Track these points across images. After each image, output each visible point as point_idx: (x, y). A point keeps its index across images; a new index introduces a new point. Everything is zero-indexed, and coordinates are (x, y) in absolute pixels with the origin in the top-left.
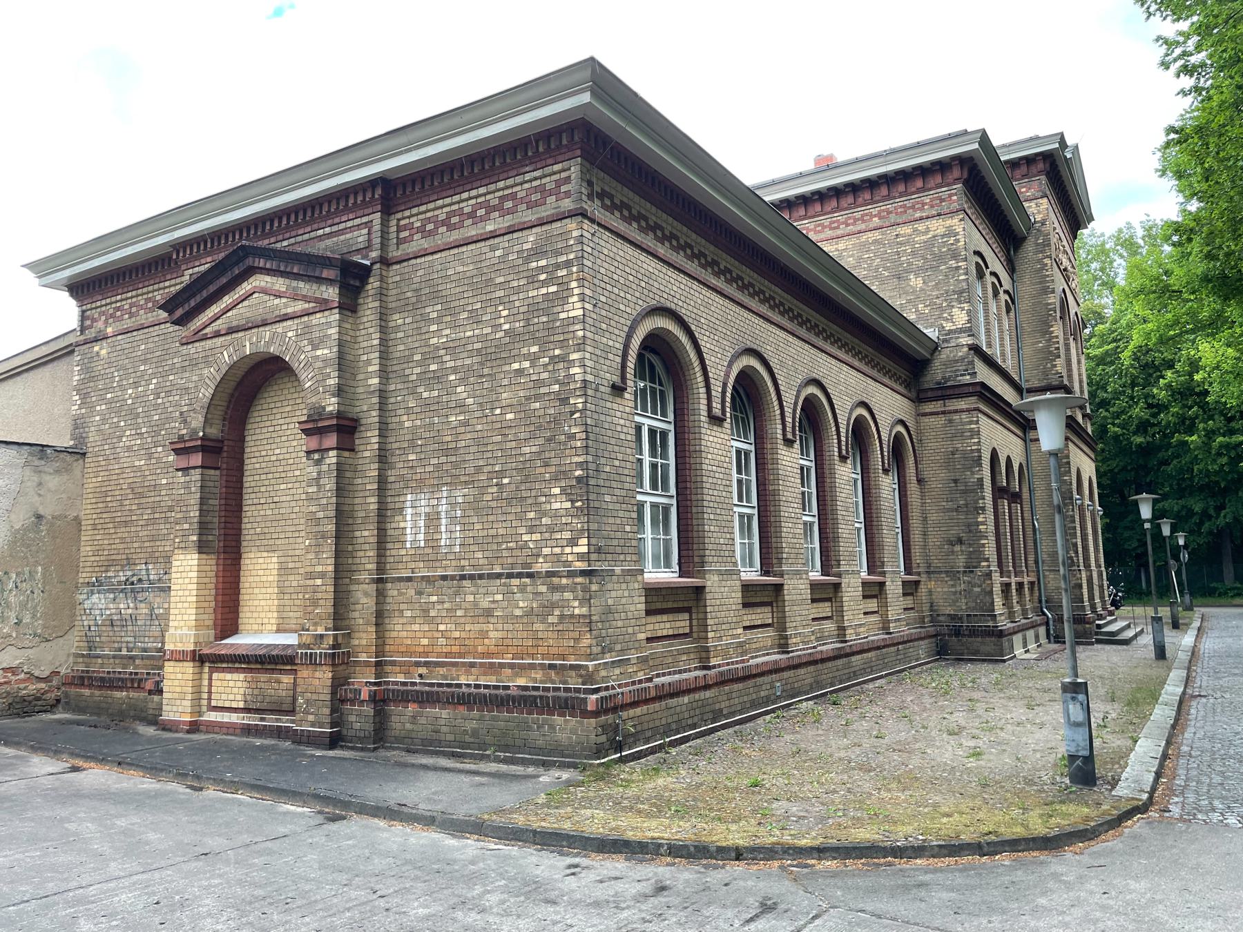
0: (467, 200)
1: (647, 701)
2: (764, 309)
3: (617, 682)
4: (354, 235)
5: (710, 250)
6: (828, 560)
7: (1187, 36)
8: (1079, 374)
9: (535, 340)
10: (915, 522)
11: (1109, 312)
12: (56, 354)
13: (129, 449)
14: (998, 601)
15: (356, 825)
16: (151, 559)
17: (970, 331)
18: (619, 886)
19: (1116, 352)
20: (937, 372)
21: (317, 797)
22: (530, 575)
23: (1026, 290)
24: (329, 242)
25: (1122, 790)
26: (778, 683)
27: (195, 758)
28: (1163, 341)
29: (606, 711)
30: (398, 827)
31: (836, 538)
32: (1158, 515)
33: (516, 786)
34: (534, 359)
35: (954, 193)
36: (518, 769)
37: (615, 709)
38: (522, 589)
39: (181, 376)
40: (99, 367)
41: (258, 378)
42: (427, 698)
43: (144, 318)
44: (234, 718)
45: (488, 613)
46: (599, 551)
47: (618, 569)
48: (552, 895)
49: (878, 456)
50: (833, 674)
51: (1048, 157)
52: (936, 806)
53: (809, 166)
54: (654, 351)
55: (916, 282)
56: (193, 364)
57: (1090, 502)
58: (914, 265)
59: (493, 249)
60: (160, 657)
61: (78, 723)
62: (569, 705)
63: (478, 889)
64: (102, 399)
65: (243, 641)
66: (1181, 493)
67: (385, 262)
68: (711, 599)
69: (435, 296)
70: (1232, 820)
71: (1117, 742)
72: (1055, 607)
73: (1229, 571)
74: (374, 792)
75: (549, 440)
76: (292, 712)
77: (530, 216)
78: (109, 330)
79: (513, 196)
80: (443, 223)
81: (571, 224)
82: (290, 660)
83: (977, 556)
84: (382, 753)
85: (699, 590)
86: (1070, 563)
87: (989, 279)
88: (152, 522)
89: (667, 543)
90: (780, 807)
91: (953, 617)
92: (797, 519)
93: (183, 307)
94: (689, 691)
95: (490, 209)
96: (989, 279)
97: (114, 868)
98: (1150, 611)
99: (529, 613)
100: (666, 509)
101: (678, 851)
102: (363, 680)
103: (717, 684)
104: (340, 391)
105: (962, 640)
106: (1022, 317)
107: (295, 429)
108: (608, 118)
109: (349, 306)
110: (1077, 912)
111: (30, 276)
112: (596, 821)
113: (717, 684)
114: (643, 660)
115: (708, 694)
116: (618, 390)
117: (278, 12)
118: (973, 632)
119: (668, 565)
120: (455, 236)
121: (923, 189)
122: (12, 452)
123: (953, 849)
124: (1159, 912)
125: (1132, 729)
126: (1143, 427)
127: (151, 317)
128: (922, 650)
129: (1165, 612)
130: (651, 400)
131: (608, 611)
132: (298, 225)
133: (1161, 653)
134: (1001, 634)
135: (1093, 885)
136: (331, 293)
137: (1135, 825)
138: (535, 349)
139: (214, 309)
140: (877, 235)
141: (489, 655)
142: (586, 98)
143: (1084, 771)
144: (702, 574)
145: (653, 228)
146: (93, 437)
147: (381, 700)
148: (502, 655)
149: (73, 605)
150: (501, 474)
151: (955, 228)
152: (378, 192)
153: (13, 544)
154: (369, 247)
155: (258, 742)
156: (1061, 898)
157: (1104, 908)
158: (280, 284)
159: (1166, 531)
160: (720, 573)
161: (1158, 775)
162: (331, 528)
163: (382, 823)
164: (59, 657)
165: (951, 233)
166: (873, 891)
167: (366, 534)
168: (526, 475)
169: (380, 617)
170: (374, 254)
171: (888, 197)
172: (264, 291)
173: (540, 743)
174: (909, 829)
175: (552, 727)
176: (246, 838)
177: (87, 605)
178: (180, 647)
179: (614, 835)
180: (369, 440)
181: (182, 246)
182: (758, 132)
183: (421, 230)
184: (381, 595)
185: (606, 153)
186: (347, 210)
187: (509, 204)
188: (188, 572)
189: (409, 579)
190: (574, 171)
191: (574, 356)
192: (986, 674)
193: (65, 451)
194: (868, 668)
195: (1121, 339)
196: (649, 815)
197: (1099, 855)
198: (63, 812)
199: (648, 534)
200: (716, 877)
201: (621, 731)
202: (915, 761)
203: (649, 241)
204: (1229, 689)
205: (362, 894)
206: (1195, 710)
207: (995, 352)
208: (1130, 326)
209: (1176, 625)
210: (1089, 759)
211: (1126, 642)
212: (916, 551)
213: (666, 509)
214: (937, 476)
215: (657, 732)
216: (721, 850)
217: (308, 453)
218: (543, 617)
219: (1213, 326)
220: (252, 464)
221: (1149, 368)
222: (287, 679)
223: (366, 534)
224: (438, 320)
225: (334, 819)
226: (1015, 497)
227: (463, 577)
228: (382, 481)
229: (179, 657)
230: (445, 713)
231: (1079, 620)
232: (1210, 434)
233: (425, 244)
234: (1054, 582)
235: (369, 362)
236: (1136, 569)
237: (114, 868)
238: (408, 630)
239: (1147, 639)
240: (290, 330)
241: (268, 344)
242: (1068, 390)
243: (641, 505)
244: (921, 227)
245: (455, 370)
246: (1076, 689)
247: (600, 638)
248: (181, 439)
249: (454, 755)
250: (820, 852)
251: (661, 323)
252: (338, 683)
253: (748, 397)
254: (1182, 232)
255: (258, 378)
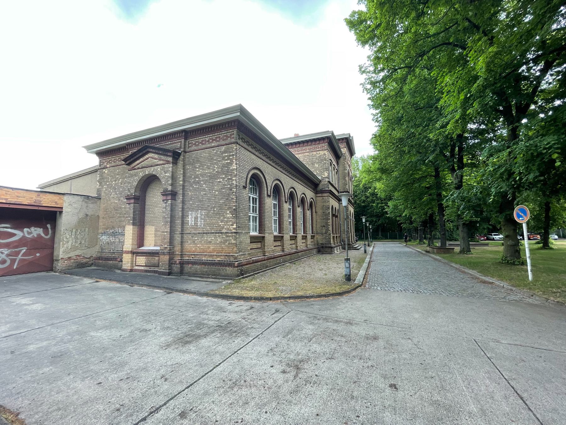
0: (207, 137)
1: (250, 264)
2: (281, 170)
3: (243, 259)
4: (177, 144)
5: (268, 154)
6: (294, 231)
7: (378, 114)
8: (351, 189)
9: (224, 174)
10: (314, 222)
11: (358, 175)
12: (93, 171)
13: (113, 198)
14: (332, 240)
15: (175, 295)
16: (120, 227)
17: (328, 178)
18: (242, 307)
19: (359, 184)
20: (320, 187)
21: (164, 288)
22: (221, 233)
23: (341, 169)
24: (170, 146)
25: (356, 282)
26: (281, 259)
27: (132, 278)
28: (369, 182)
29: (240, 266)
30: (186, 295)
31: (296, 225)
32: (366, 221)
33: (216, 284)
34: (223, 179)
35: (326, 145)
36: (217, 280)
37: (242, 266)
38: (219, 236)
39: (131, 179)
40: (105, 175)
41: (149, 181)
42: (194, 263)
43: (118, 163)
44: (142, 268)
45: (210, 242)
46: (239, 227)
47: (243, 232)
48: (225, 310)
49: (306, 207)
50: (294, 257)
51: (346, 138)
52: (316, 287)
53: (293, 136)
54: (254, 178)
55: (317, 165)
56: (132, 176)
57: (352, 218)
58: (315, 161)
59: (213, 150)
60: (122, 252)
61: (98, 269)
62: (230, 265)
63: (206, 309)
64: (106, 184)
65: (145, 248)
66: (371, 216)
67: (185, 152)
68: (266, 240)
69: (198, 161)
70: (379, 288)
71: (356, 271)
72: (344, 241)
73: (380, 233)
74: (185, 287)
75: (227, 199)
76: (158, 266)
77: (223, 143)
78: (108, 166)
79: (219, 137)
80: (201, 143)
81: (234, 145)
82: (158, 253)
83: (327, 230)
84: (182, 277)
85: (264, 237)
86: (347, 232)
87: (333, 166)
88: (119, 217)
89: (256, 226)
90: (281, 288)
91: (322, 244)
92: (287, 220)
93: (129, 161)
94: (260, 261)
95: (213, 140)
96: (333, 166)
97: (107, 307)
98: (364, 243)
99: (221, 242)
100: (256, 217)
101: (256, 299)
102: (177, 259)
103: (267, 259)
104: (172, 185)
105: (323, 249)
106: (340, 175)
107: (159, 194)
108: (244, 119)
109: (175, 162)
110: (346, 309)
111: (85, 150)
112: (236, 292)
113: (267, 259)
114: (249, 254)
115: (265, 262)
116: (245, 187)
117: (159, 86)
118: (326, 247)
119: (256, 231)
120: (204, 146)
121: (319, 144)
122: (79, 197)
123: (320, 296)
124: (363, 309)
125: (359, 269)
126: (364, 201)
127: (120, 163)
128: (315, 251)
129: (367, 243)
130: (253, 190)
131: (241, 242)
132: (161, 141)
133: (365, 252)
134: (332, 248)
135: (349, 303)
136: (170, 159)
137: (359, 290)
138: (224, 176)
139: (138, 162)
140: (308, 154)
141: (210, 252)
142: (239, 114)
143: (348, 278)
144: (264, 233)
145: (255, 148)
146: (103, 194)
147: (182, 264)
148: (214, 252)
149: (97, 239)
150: (214, 208)
151: (327, 154)
152: (183, 134)
153: (79, 222)
154: (181, 148)
155: (149, 274)
156: (342, 306)
157: (351, 308)
158: (156, 156)
159: (368, 225)
160: (268, 233)
161: (364, 278)
162: (169, 220)
163: (182, 294)
164: (93, 252)
165: (325, 154)
166: (301, 306)
167: (179, 222)
168: (221, 207)
169: (182, 243)
170: (182, 150)
171: (311, 145)
172: (152, 158)
173: (223, 274)
174: (310, 292)
175: (226, 270)
176: (145, 298)
177: (101, 238)
178: (127, 250)
179: (241, 295)
180: (180, 198)
181: (128, 144)
182: (282, 126)
183: (195, 144)
184: (182, 237)
185: (241, 128)
186: (175, 138)
187: (218, 139)
188: (130, 231)
189: (190, 233)
190: (235, 132)
191: (234, 178)
192: (328, 257)
193: (95, 198)
194: (302, 255)
195: (361, 181)
196: (250, 291)
197: (352, 296)
198: (94, 293)
199: (251, 223)
200: (265, 304)
201: (243, 271)
202: (312, 277)
203: (253, 151)
204: (379, 260)
205: (176, 311)
206: (372, 264)
207: (333, 183)
208: (362, 179)
209: (369, 246)
210: (350, 275)
211: (358, 249)
212: (314, 228)
213: (256, 217)
214: (320, 211)
215: (254, 271)
216: (266, 298)
217: (163, 200)
218: (224, 243)
219: (379, 180)
220: (148, 203)
221: (366, 188)
222: (157, 258)
223: (179, 222)
224: (199, 168)
225: (169, 293)
226: (337, 217)
227: (204, 233)
228: (183, 208)
229: (127, 252)
230: (199, 267)
231: (349, 244)
232: (378, 204)
233: (196, 148)
234: (344, 236)
235: (180, 177)
236: (361, 233)
237: (107, 307)
238: (189, 246)
239: (363, 249)
240: (159, 168)
241: (153, 172)
242: (349, 192)
243: (250, 216)
244: (318, 152)
245: (203, 181)
246: (348, 260)
247: (239, 249)
248: (128, 196)
249: (201, 277)
250: (290, 298)
251: (256, 171)
252: (171, 259)
253: (277, 191)
254: (374, 158)
255: (149, 181)
